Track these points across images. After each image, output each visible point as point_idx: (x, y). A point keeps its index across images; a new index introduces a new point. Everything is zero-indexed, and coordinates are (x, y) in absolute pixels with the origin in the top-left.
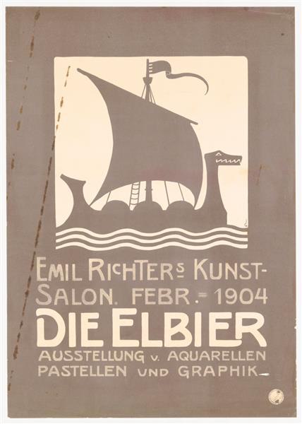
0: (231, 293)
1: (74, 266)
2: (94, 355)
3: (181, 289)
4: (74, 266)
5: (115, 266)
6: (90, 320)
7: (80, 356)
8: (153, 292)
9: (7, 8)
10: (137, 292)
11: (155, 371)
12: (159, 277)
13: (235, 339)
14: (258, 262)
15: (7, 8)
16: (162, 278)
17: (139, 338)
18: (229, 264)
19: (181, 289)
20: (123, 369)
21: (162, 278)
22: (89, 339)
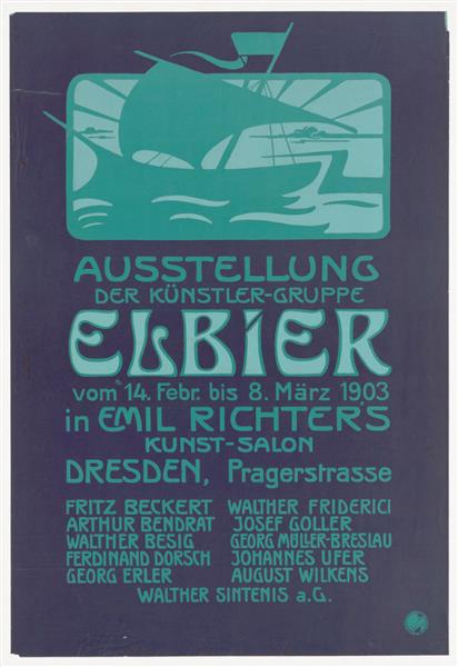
0: (354, 387)
1: (68, 429)
2: (219, 267)
3: (68, 475)
4: (68, 429)
5: (293, 449)
6: (172, 464)
7: (208, 296)
8: (118, 465)
9: (447, 654)
10: (113, 465)
11: (194, 464)
12: (335, 426)
13: (332, 153)
14: (314, 445)
15: (447, 654)
16: (339, 428)
17: (265, 274)
18: (314, 441)
19: (68, 475)
20: (194, 464)
21: (339, 428)
22: (251, 274)
